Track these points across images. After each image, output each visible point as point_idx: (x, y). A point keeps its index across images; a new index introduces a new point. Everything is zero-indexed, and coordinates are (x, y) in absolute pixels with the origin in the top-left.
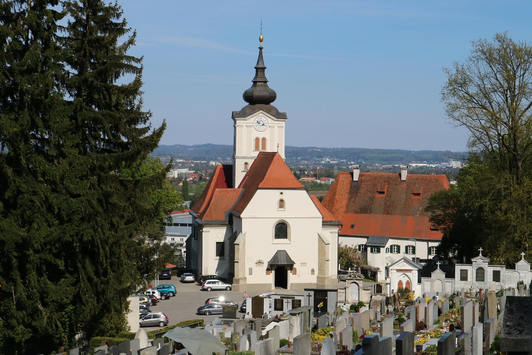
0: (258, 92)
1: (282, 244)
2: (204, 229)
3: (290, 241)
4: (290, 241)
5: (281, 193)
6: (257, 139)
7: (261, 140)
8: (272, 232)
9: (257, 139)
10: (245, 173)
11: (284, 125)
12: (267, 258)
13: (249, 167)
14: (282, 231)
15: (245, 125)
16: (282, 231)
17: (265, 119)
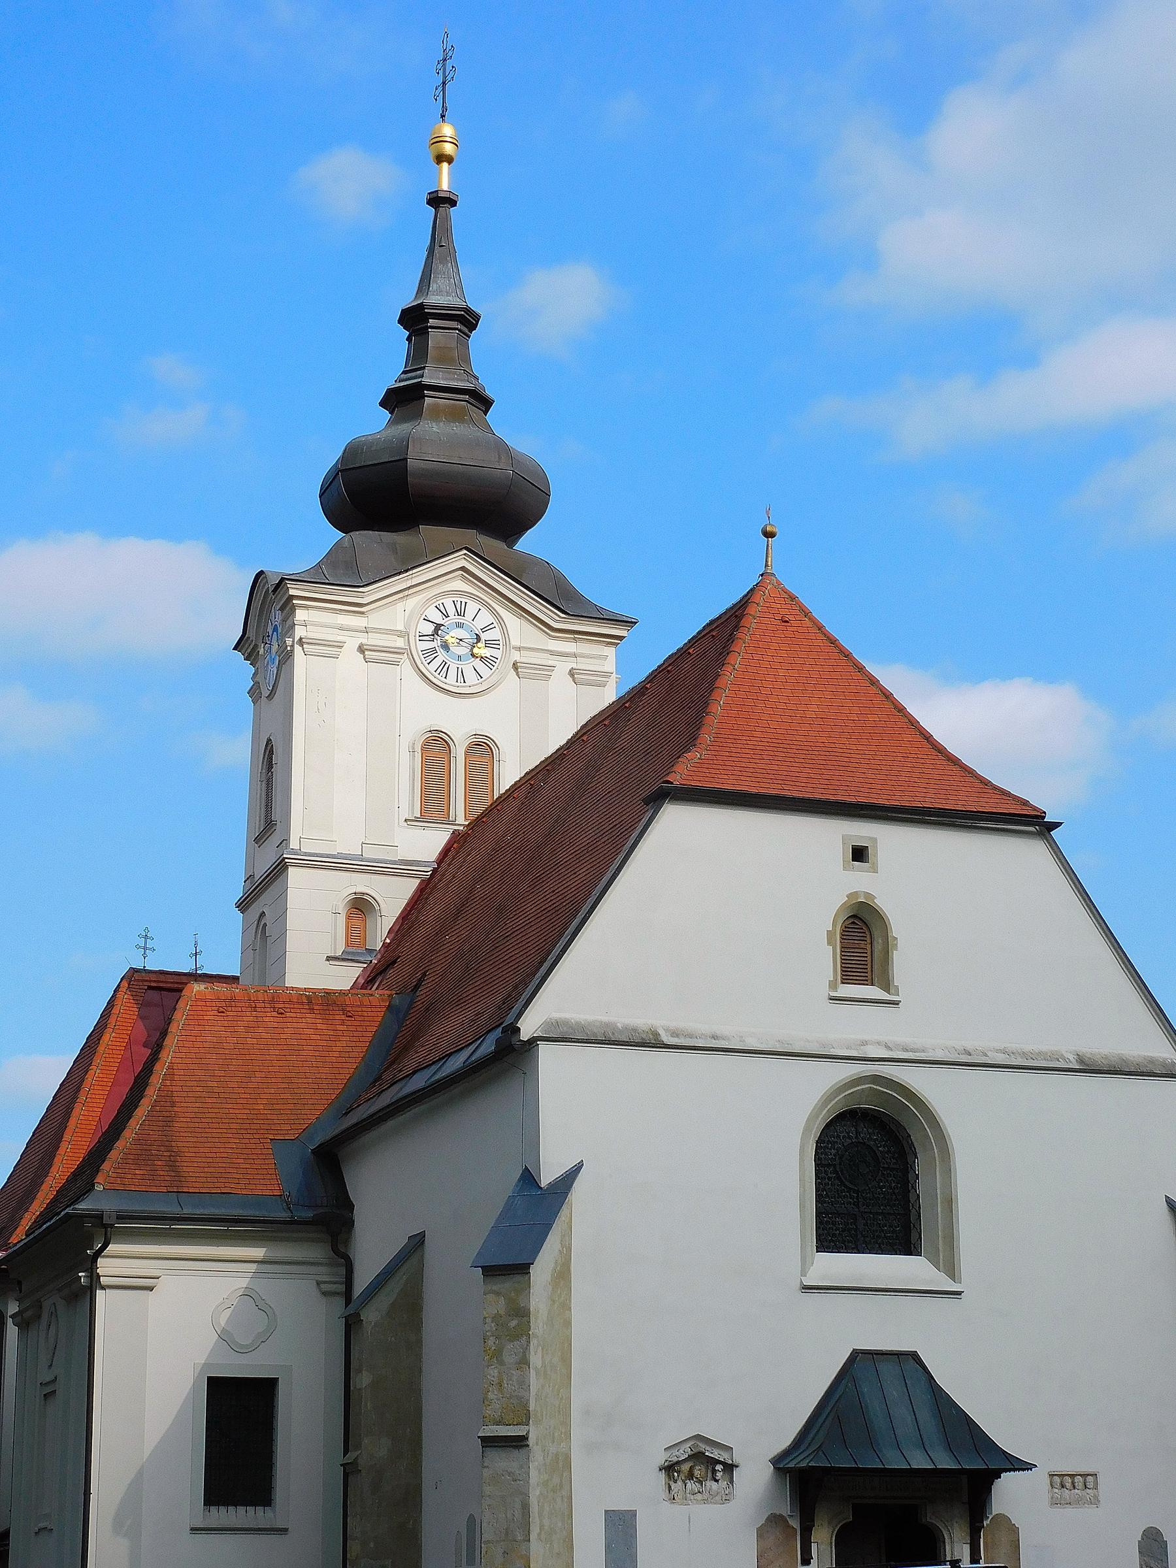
0: (435, 442)
1: (875, 1303)
2: (117, 1262)
3: (951, 1271)
4: (951, 1271)
5: (859, 854)
6: (436, 745)
7: (459, 752)
8: (786, 1183)
9: (436, 745)
10: (415, 883)
11: (610, 665)
12: (766, 1417)
13: (380, 931)
14: (872, 1175)
15: (352, 643)
16: (872, 1175)
17: (485, 618)
